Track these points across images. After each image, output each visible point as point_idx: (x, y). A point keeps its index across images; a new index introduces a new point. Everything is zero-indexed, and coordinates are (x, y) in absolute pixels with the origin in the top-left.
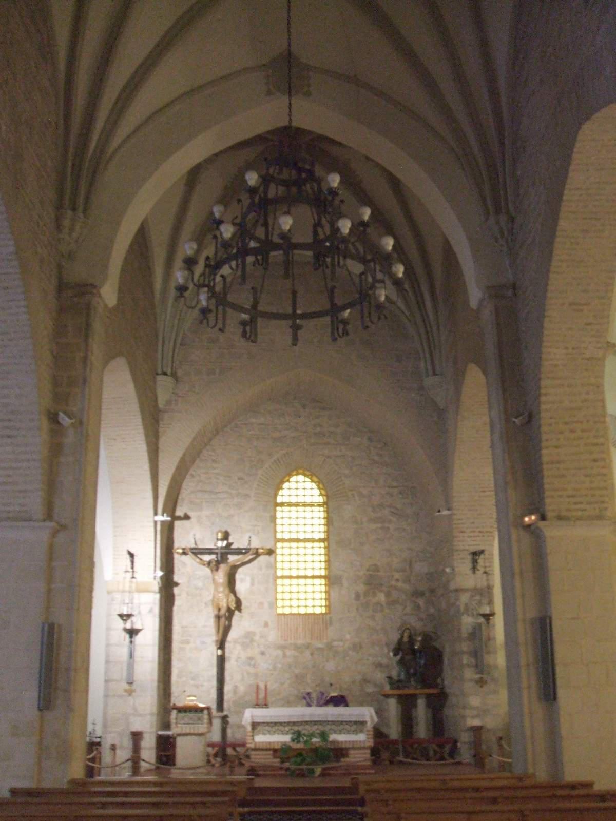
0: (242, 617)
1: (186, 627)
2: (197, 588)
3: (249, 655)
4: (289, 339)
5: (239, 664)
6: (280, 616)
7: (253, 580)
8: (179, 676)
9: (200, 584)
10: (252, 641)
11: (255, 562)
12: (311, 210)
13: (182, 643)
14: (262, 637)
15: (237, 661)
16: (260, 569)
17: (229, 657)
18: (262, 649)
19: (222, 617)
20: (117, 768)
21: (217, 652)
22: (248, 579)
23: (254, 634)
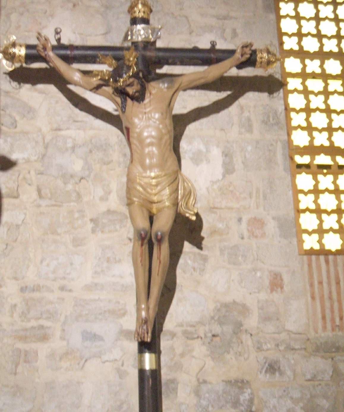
0: (205, 259)
1: (37, 288)
2: (67, 177)
3: (233, 375)
4: (103, 32)
5: (204, 403)
6: (314, 257)
7: (227, 155)
8: (185, 108)
9: (77, 166)
10: (238, 328)
11: (233, 109)
12: (49, 59)
13: (24, 339)
14: (266, 319)
15: (197, 393)
16: (248, 127)
17: (173, 381)
18: (273, 355)
19: (160, 241)
20: (25, 221)
21: (141, 361)
22: (216, 153)
23: (245, 310)
